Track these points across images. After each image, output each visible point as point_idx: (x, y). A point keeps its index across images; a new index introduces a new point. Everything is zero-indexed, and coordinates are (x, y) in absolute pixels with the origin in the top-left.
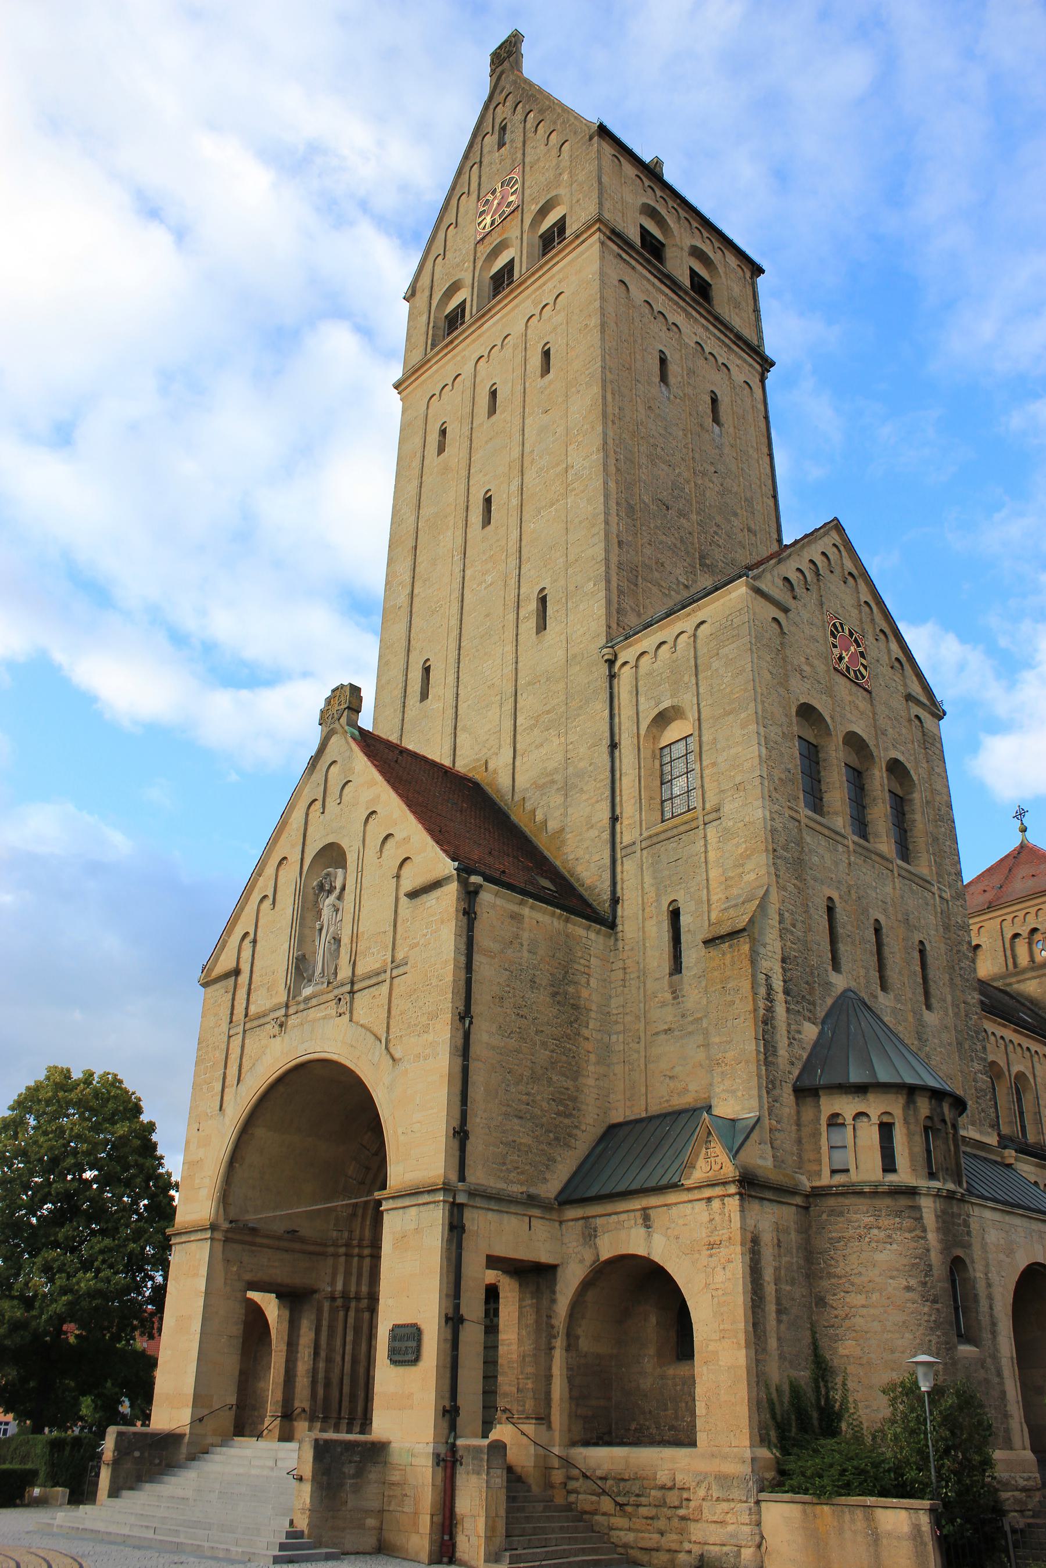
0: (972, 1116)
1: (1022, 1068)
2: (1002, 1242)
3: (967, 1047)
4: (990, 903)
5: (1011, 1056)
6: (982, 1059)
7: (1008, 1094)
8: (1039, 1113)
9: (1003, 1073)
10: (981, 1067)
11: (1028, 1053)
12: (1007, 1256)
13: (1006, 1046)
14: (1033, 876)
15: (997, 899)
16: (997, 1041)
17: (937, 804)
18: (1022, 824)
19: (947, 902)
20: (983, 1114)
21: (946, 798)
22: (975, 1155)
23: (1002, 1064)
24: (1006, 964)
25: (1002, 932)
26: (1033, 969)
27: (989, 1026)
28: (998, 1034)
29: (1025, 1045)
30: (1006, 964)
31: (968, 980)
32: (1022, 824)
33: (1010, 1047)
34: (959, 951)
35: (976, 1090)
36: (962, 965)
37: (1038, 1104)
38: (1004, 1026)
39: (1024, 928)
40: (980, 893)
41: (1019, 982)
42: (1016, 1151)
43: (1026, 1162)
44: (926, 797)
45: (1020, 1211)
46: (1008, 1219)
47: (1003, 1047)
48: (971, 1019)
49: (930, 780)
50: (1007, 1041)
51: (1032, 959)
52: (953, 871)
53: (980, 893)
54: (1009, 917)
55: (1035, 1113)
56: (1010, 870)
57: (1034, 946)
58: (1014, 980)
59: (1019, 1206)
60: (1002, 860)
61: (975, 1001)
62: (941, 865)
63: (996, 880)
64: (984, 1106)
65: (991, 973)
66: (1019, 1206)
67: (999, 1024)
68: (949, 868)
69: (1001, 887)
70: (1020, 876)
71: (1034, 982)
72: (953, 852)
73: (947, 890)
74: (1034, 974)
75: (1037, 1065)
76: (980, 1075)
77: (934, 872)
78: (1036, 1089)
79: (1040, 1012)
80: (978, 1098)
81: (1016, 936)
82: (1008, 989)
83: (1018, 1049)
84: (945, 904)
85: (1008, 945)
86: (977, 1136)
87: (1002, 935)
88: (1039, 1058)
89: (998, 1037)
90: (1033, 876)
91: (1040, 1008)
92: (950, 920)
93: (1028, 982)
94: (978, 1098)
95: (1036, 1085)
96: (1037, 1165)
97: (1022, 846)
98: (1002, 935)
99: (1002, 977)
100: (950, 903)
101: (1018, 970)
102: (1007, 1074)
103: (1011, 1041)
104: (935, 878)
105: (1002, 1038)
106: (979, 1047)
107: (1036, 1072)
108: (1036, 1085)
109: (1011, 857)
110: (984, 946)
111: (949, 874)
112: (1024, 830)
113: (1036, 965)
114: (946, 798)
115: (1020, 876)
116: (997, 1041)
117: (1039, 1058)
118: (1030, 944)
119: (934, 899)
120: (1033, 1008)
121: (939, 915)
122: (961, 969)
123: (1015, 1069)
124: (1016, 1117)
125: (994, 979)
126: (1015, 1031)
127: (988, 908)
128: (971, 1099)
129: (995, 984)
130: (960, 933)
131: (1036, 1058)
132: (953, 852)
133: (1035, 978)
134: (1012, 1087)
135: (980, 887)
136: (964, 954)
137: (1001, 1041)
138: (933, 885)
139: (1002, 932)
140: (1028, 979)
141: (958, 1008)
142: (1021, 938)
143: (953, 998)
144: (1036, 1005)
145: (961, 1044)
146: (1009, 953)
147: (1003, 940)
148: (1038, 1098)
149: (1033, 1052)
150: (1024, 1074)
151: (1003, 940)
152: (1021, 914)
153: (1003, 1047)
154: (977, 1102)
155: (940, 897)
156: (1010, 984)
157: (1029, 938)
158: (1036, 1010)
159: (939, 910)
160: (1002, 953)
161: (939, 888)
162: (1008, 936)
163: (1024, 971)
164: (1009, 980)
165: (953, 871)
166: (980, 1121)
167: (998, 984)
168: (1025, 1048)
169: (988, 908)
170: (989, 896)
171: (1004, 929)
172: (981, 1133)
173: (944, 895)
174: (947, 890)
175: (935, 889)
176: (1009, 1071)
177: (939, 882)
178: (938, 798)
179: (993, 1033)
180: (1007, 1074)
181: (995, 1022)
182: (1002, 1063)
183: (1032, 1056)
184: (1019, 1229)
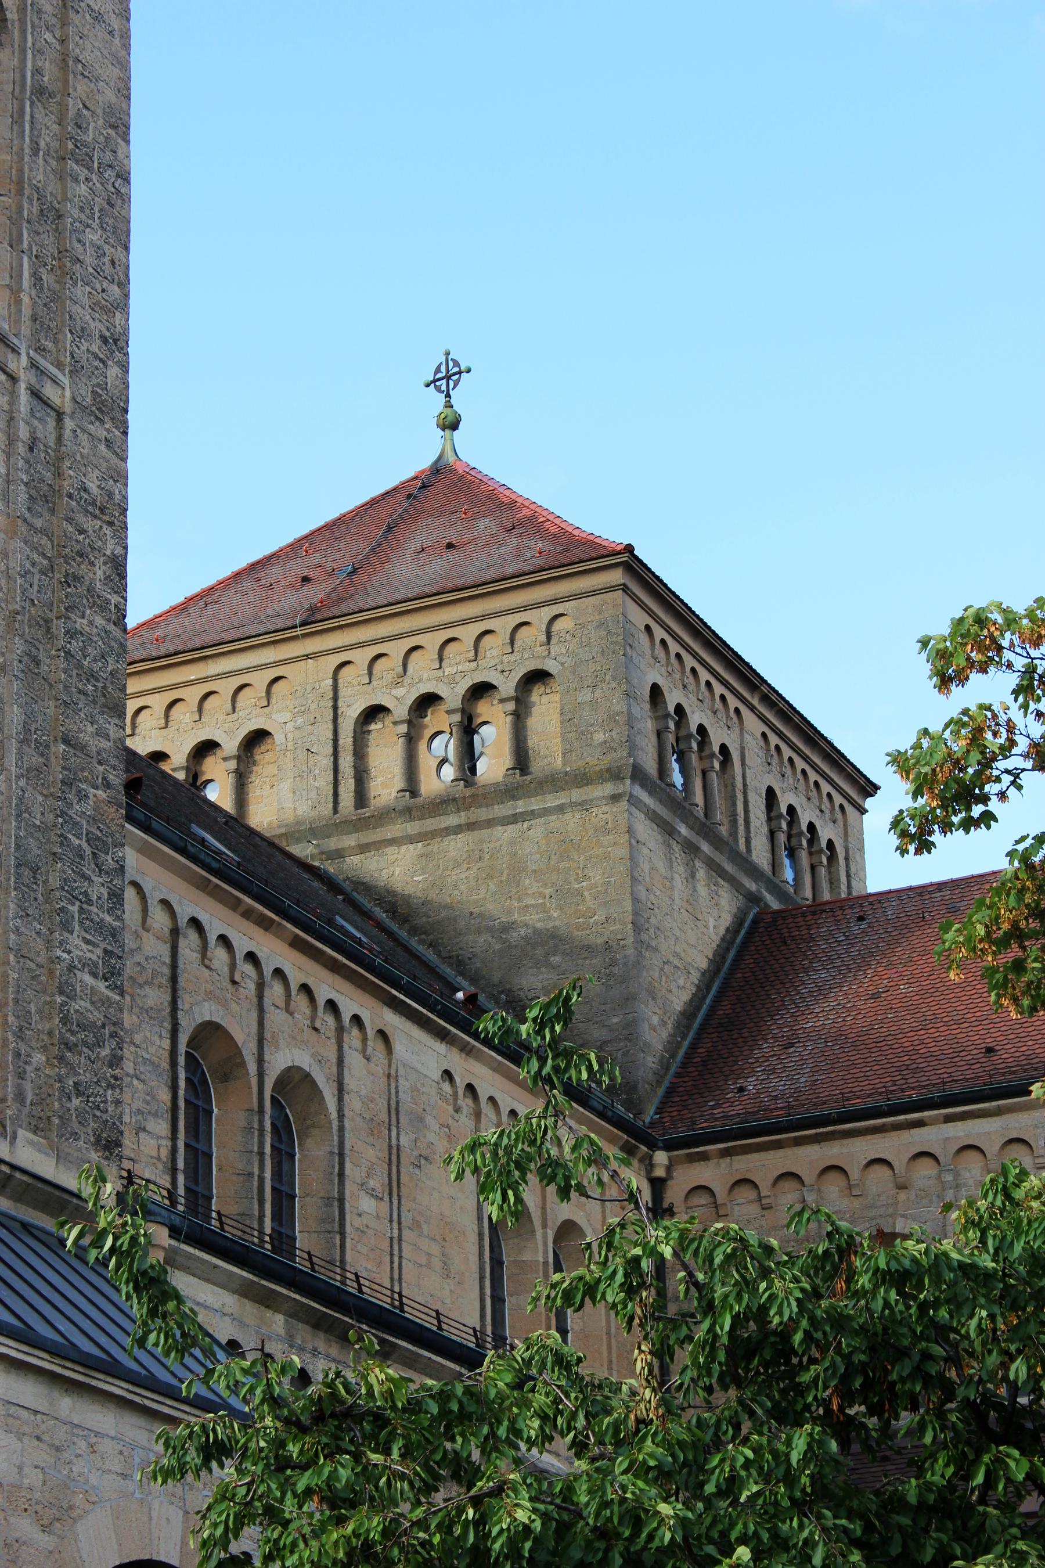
0: (40, 1101)
1: (304, 1060)
2: (33, 1478)
3: (54, 881)
4: (313, 609)
5: (276, 1018)
6: (100, 927)
7: (249, 1129)
8: (341, 1201)
9: (243, 1064)
10: (95, 955)
11: (330, 1020)
12: (45, 1528)
13: (261, 986)
14: (450, 546)
15: (341, 600)
16: (233, 966)
17: (73, 106)
18: (449, 405)
19: (60, 416)
20: (76, 1102)
21: (110, 96)
22: (25, 1226)
23: (239, 1037)
24: (336, 794)
25: (335, 698)
26: (408, 813)
27: (127, 825)
28: (242, 944)
29: (323, 993)
30: (336, 794)
31: (92, 676)
32: (449, 405)
33: (275, 991)
34: (77, 578)
35: (65, 1020)
36: (81, 623)
37: (341, 1174)
38: (265, 924)
39: (400, 692)
40: (291, 586)
41: (364, 848)
42: (175, 1232)
43: (208, 1277)
44: (38, 71)
45: (118, 1388)
46: (66, 1404)
47: (252, 986)
48: (82, 797)
49: (64, 23)
50: (268, 971)
51: (412, 787)
52: (96, 327)
53: (291, 586)
54: (361, 657)
55: (328, 1201)
56: (389, 529)
57: (422, 745)
58: (349, 841)
59: (112, 1369)
60: (374, 502)
61: (106, 744)
62: (56, 297)
63: (344, 554)
64: (85, 1077)
65: (289, 817)
66: (112, 1369)
67: (248, 914)
68: (83, 315)
69: (355, 571)
70: (415, 545)
71: (408, 853)
72: (108, 268)
73: (66, 381)
74: (412, 828)
75: (353, 1059)
76: (88, 979)
77: (26, 311)
78: (341, 1129)
79: (413, 942)
80: (69, 1047)
81: (374, 712)
82: (330, 868)
83: (301, 1002)
84: (51, 423)
85: (346, 739)
86: (46, 1167)
87: (335, 708)
88: (365, 1040)
89: (240, 955)
90: (450, 546)
91: (414, 931)
92: (59, 474)
93: (390, 850)
94: (69, 1047)
95: (341, 1116)
96: (246, 1291)
97: (439, 470)
98: (335, 708)
99: (315, 831)
100: (69, 424)
101: (366, 812)
102: (252, 1068)
103: (278, 972)
104: (26, 329)
105: (251, 957)
106: (98, 889)
107: (347, 1079)
108: (341, 1116)
109: (401, 497)
110: (278, 737)
111: (82, 333)
112: (451, 424)
113: (419, 800)
114: (110, 96)
115: (415, 545)
116: (233, 966)
117: (365, 1040)
118: (411, 740)
119: (13, 394)
120: (394, 927)
121: (21, 449)
122: (72, 634)
123: (279, 1060)
124: (261, 1202)
125: (295, 833)
126: (296, 944)
127: (303, 624)
128: (45, 1049)
129: (298, 850)
130: (90, 524)
131: (353, 1038)
132: (108, 268)
133: (411, 839)
134: (261, 1111)
135: (298, 568)
136: (90, 590)
137: (248, 969)
138: (15, 351)
139: (335, 698)
140: (393, 842)
141: (43, 749)
142: (388, 720)
143: (29, 717)
144: (404, 920)
145: (35, 870)
146: (347, 761)
147: (335, 720)
148: (341, 1155)
149: (346, 1018)
150: (307, 1077)
151: (335, 720)
152: (396, 650)
153: (251, 987)
154: (61, 1058)
155: (36, 394)
156: (339, 854)
157: (410, 722)
158: (403, 934)
159: (24, 433)
160: (327, 762)
161: (33, 365)
162: (352, 710)
163: (384, 816)
164: (333, 843)
165: (96, 327)
166: (64, 1121)
167: (302, 850)
168: (321, 1002)
169: (303, 624)
170: (314, 594)
171: (343, 692)
172: (61, 1158)
173: (49, 391)
174: (66, 381)
175: (19, 364)
176: (260, 1061)
177: (41, 350)
178: (80, 88)
179: (223, 939)
180: (252, 1068)
181: (234, 905)
182: (243, 1034)
183: (340, 1030)
184: (107, 1446)
